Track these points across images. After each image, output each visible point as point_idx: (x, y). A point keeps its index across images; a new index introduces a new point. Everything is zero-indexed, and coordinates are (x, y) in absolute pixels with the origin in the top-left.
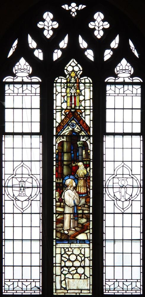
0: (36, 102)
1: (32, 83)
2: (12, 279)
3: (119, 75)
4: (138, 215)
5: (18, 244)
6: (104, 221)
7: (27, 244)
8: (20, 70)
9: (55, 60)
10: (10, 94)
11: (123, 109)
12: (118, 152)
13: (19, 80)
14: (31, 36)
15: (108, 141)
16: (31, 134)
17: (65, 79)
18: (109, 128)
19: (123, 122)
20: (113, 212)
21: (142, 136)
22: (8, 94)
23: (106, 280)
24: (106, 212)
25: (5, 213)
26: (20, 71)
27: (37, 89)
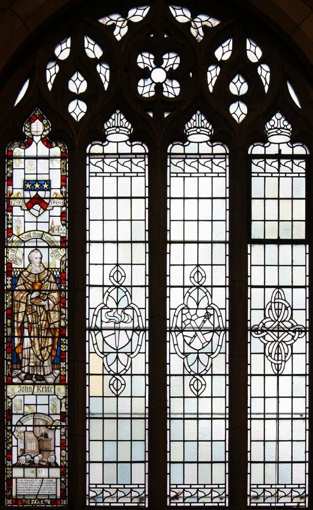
0: (221, 186)
1: (292, 157)
2: (209, 485)
4: (261, 377)
6: (249, 387)
8: (195, 129)
11: (184, 198)
13: (272, 150)
15: (256, 253)
16: (293, 242)
17: (211, 145)
18: (257, 232)
21: (307, 246)
22: (175, 175)
23: (172, 486)
25: (170, 375)
26: (195, 132)
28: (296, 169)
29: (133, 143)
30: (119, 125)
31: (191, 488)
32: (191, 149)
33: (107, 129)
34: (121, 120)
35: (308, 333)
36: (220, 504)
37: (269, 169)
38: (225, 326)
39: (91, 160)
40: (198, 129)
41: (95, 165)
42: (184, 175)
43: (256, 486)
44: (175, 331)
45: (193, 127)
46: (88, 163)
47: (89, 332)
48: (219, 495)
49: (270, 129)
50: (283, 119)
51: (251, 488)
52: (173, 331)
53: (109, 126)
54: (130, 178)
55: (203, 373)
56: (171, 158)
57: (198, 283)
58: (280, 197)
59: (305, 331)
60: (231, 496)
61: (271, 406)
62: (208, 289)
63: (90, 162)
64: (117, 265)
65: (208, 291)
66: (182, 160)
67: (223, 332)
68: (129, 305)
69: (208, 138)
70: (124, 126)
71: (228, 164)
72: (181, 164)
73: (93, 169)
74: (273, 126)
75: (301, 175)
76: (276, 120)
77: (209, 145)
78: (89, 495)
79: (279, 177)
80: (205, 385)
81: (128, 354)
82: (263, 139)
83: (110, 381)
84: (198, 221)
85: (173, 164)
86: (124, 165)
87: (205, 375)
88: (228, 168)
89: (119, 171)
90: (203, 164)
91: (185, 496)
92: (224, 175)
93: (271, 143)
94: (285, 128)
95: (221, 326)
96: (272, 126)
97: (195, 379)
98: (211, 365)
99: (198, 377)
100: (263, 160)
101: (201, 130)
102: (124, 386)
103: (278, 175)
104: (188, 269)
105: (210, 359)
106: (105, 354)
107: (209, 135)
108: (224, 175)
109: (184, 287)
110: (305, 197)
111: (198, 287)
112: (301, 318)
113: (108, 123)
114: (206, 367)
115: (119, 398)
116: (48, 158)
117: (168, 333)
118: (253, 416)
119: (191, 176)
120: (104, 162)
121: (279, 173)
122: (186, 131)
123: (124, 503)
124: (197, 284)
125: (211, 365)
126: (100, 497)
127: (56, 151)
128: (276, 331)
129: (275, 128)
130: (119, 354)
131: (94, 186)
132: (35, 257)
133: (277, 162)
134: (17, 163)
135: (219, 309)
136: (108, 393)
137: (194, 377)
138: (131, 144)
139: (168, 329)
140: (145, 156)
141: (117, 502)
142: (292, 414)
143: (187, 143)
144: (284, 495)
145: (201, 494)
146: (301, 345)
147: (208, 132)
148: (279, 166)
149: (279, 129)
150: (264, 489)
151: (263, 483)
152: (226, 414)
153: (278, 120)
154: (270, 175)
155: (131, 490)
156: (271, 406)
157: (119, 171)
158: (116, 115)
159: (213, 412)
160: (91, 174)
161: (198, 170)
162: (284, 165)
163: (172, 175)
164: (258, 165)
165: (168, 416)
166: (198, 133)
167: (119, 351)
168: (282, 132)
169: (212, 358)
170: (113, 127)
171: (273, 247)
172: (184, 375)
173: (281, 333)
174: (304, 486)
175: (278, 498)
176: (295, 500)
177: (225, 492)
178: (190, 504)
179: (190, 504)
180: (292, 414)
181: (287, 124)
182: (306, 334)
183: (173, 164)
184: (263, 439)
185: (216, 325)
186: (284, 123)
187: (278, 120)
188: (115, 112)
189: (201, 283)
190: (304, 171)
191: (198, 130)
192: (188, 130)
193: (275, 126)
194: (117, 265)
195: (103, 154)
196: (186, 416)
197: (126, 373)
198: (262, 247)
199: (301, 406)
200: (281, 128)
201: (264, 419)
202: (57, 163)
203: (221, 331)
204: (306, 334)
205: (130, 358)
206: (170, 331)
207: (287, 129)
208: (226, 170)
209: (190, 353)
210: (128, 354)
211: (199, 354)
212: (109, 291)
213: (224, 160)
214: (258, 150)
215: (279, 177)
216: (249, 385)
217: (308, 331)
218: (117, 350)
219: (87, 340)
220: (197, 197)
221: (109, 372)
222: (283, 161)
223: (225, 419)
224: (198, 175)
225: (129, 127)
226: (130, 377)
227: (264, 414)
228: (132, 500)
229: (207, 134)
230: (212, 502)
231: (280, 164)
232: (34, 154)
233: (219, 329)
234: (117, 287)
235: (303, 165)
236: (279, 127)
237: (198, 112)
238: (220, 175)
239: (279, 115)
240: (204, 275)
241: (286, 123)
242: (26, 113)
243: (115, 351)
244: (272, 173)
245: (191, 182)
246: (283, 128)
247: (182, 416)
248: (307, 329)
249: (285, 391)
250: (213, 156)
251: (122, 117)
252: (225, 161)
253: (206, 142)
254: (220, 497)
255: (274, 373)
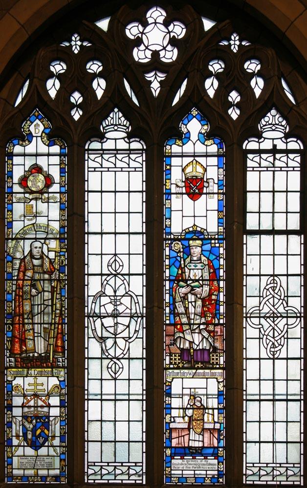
0: (138, 181)
1: (287, 152)
3: (264, 135)
5: (280, 436)
7: (267, 435)
8: (113, 126)
9: (78, 118)
10: (97, 170)
12: (267, 261)
13: (267, 145)
14: (30, 80)
15: (251, 244)
16: (287, 232)
17: (128, 141)
18: (252, 222)
19: (194, 216)
20: (258, 357)
24: (248, 357)
26: (113, 129)
27: (138, 161)
28: (291, 163)
29: (131, 140)
30: (117, 123)
31: (108, 466)
32: (109, 145)
33: (106, 127)
34: (119, 118)
35: (302, 318)
36: (137, 482)
37: (264, 164)
38: (142, 312)
39: (90, 156)
40: (116, 126)
41: (94, 161)
42: (101, 169)
43: (252, 465)
44: (93, 317)
45: (110, 124)
46: (86, 158)
47: (88, 318)
48: (137, 473)
49: (264, 126)
50: (278, 116)
51: (246, 467)
52: (91, 317)
53: (107, 124)
54: (100, 173)
55: (121, 357)
56: (88, 154)
57: (116, 271)
58: (288, 190)
59: (142, 317)
60: (149, 473)
61: (267, 388)
62: (125, 277)
63: (88, 157)
64: (115, 255)
65: (125, 279)
66: (100, 155)
67: (140, 319)
68: (126, 293)
69: (125, 135)
70: (122, 124)
71: (144, 159)
72: (99, 160)
73: (92, 164)
74: (268, 122)
75: (251, 169)
76: (271, 117)
77: (283, 142)
78: (87, 473)
79: (274, 171)
80: (123, 368)
81: (126, 339)
82: (101, 137)
83: (108, 364)
84: (115, 213)
85: (132, 159)
86: (254, 160)
87: (123, 358)
88: (144, 163)
89: (289, 166)
90: (292, 159)
91: (102, 473)
92: (141, 169)
93: (265, 138)
94: (280, 124)
95: (138, 312)
96: (266, 122)
97: (112, 362)
98: (129, 349)
99: (115, 360)
100: (285, 155)
101: (118, 128)
102: (122, 369)
103: (273, 169)
104: (106, 259)
105: (127, 343)
106: (102, 340)
107: (126, 133)
108: (141, 169)
109: (102, 275)
110: (299, 190)
111: (115, 275)
112: (296, 303)
113: (106, 121)
114: (124, 351)
115: (117, 381)
116: (49, 155)
117: (86, 318)
118: (90, 397)
119: (108, 171)
120: (102, 157)
121: (274, 167)
122: (104, 128)
123: (108, 480)
124: (114, 273)
125: (129, 349)
126: (99, 474)
127: (56, 149)
128: (271, 317)
129: (269, 124)
130: (117, 339)
131: (93, 181)
132: (36, 246)
133: (273, 157)
134: (175, 161)
135: (136, 296)
136: (106, 375)
137: (112, 360)
138: (129, 141)
139: (86, 315)
140: (143, 152)
141: (101, 479)
142: (115, 394)
143: (105, 140)
144: (266, 473)
145: (118, 472)
146: (297, 331)
147: (126, 130)
148: (274, 160)
149: (274, 125)
150: (115, 467)
151: (272, 462)
152: (143, 395)
153: (273, 116)
154: (107, 169)
155: (260, 469)
156: (267, 388)
157: (289, 166)
158: (114, 113)
159: (117, 393)
160: (90, 169)
161: (115, 165)
162: (279, 160)
163: (90, 169)
164: (254, 160)
165: (86, 397)
166: (116, 130)
167: (117, 336)
168: (277, 128)
169: (129, 343)
170: (112, 125)
171: (283, 238)
172: (101, 358)
173: (275, 319)
174: (141, 464)
175: (102, 476)
176: (290, 479)
177: (142, 469)
178: (108, 481)
179: (122, 481)
180: (287, 395)
181: (282, 120)
182: (300, 320)
183: (132, 159)
184: (259, 420)
185: (134, 311)
186: (278, 119)
187: (273, 116)
188: (113, 111)
189: (118, 272)
190: (299, 166)
191: (116, 128)
192: (106, 127)
193: (270, 122)
194: (115, 255)
195: (102, 150)
196: (262, 397)
197: (124, 357)
198: (285, 237)
199: (296, 388)
200: (276, 124)
201: (129, 400)
202: (56, 160)
203: (138, 317)
204: (300, 320)
205: (127, 343)
206: (89, 317)
207: (281, 125)
208: (142, 165)
209: (108, 338)
210: (126, 339)
211: (117, 339)
212: (107, 279)
213: (141, 155)
214: (252, 145)
215: (274, 171)
216: (244, 370)
217: (302, 317)
218: (115, 336)
219: (86, 325)
220: (100, 190)
221: (107, 356)
222: (278, 156)
223: (142, 400)
224: (115, 169)
225: (128, 125)
226: (128, 360)
227: (129, 394)
228: (287, 478)
229: (125, 131)
230: (259, 481)
231: (275, 159)
232: (34, 151)
233: (136, 315)
234: (115, 275)
235: (298, 159)
236: (274, 123)
237: (116, 110)
238: (137, 169)
239: (273, 112)
240: (121, 264)
241: (281, 119)
242: (25, 113)
243: (114, 336)
244: (253, 168)
245: (108, 177)
246: (278, 125)
247: (257, 397)
248: (302, 315)
249: (280, 374)
250: (130, 151)
251: (121, 115)
252: (142, 156)
253: (281, 138)
254: (138, 475)
255: (268, 357)
